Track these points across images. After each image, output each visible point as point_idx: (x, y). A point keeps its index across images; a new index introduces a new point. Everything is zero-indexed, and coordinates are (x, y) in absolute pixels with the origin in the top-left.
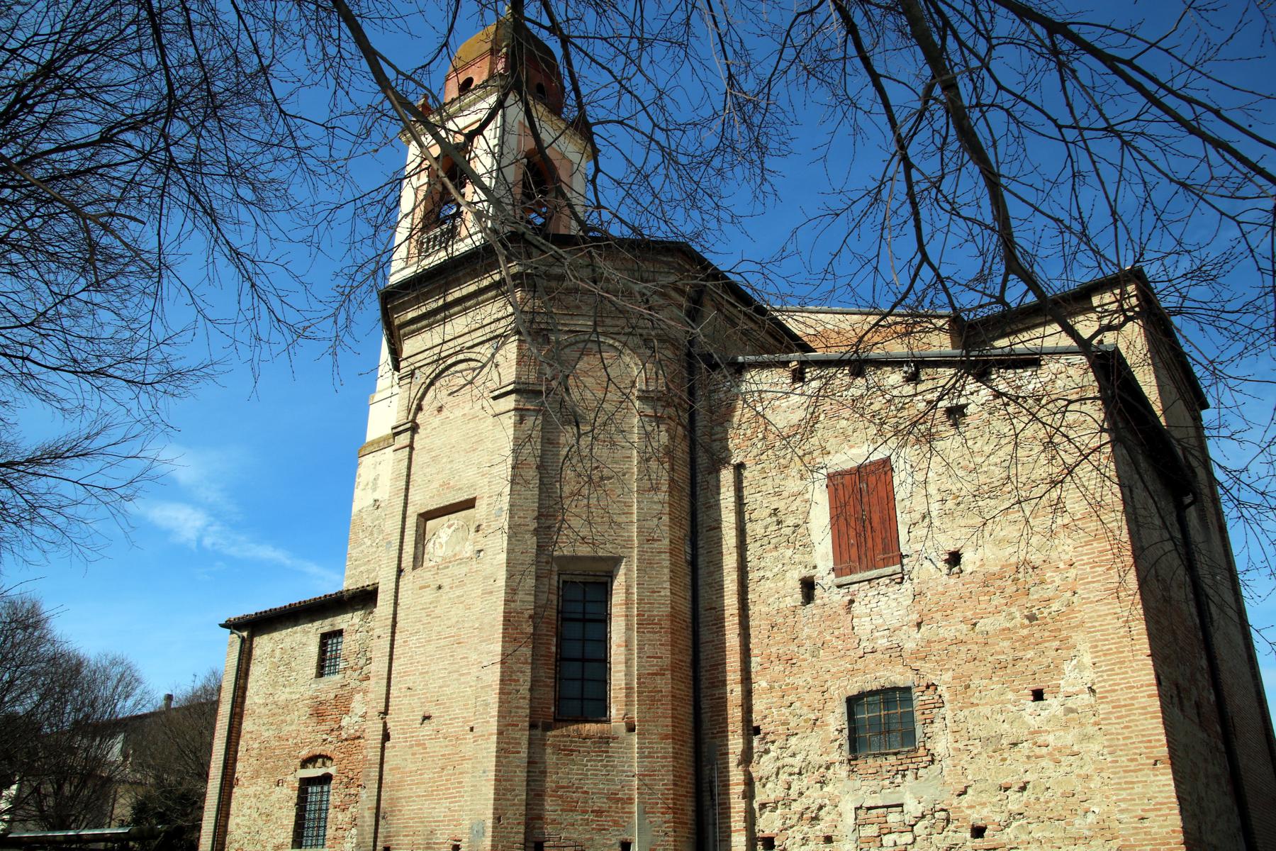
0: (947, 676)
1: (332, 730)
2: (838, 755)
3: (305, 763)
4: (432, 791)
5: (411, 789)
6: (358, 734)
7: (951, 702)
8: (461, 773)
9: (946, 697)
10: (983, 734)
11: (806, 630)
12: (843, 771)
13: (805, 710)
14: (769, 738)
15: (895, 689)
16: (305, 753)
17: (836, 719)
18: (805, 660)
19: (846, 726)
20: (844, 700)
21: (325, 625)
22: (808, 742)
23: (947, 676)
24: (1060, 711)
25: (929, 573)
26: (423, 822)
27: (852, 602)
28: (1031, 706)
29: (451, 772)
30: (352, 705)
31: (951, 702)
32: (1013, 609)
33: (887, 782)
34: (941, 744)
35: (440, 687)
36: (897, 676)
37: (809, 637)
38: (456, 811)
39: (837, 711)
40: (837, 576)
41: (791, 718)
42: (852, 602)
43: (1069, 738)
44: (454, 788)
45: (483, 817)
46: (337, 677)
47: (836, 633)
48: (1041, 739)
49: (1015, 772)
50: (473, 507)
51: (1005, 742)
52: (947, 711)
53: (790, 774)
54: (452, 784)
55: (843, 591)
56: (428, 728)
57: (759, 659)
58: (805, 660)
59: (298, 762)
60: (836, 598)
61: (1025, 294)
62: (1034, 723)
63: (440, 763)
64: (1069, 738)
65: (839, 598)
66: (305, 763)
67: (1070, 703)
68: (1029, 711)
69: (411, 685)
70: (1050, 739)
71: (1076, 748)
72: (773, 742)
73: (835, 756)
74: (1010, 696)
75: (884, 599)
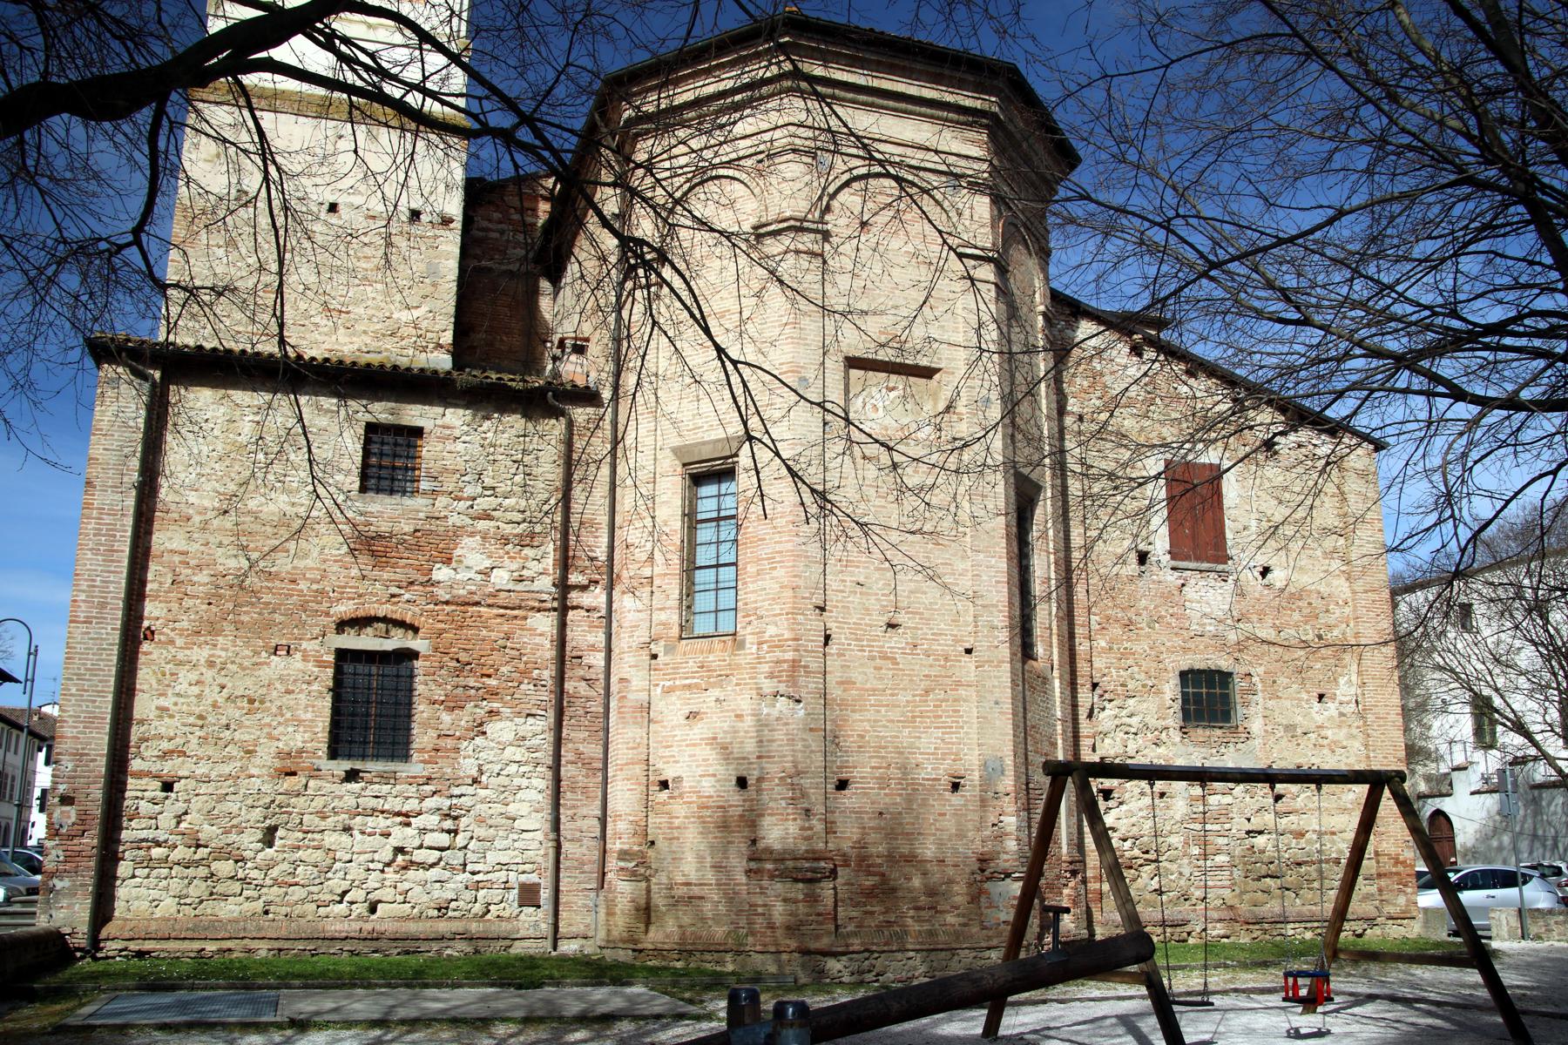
0: (1261, 670)
1: (412, 583)
2: (1173, 720)
3: (342, 625)
4: (913, 717)
5: (879, 711)
6: (476, 598)
7: (1263, 691)
8: (955, 700)
9: (1260, 686)
10: (1285, 722)
11: (1143, 601)
12: (1176, 736)
13: (1143, 676)
14: (1107, 696)
15: (1220, 672)
16: (345, 609)
17: (1171, 688)
18: (1142, 629)
19: (1179, 696)
20: (1177, 673)
21: (381, 411)
22: (1145, 705)
23: (1261, 670)
24: (1335, 713)
25: (1250, 578)
26: (902, 753)
27: (1183, 585)
28: (1317, 706)
29: (942, 697)
30: (458, 552)
31: (1263, 691)
32: (1308, 627)
33: (1214, 751)
34: (1256, 726)
35: (912, 592)
36: (1224, 664)
37: (1146, 608)
38: (953, 744)
39: (1172, 682)
40: (1173, 558)
41: (1129, 680)
42: (1183, 585)
43: (1341, 734)
44: (947, 717)
45: (999, 754)
46: (419, 502)
47: (1171, 611)
48: (1323, 733)
49: (1306, 756)
50: (930, 377)
51: (1299, 731)
52: (1259, 698)
53: (1127, 733)
54: (943, 711)
55: (1176, 574)
56: (895, 641)
57: (1097, 618)
58: (1142, 629)
59: (330, 622)
60: (1170, 578)
61: (568, 151)
62: (1319, 719)
63: (923, 685)
64: (1341, 734)
65: (1172, 578)
66: (342, 625)
67: (1342, 710)
68: (1316, 709)
69: (861, 580)
70: (1329, 733)
71: (1345, 743)
72: (1110, 701)
73: (1170, 722)
74: (1305, 696)
75: (1211, 590)
